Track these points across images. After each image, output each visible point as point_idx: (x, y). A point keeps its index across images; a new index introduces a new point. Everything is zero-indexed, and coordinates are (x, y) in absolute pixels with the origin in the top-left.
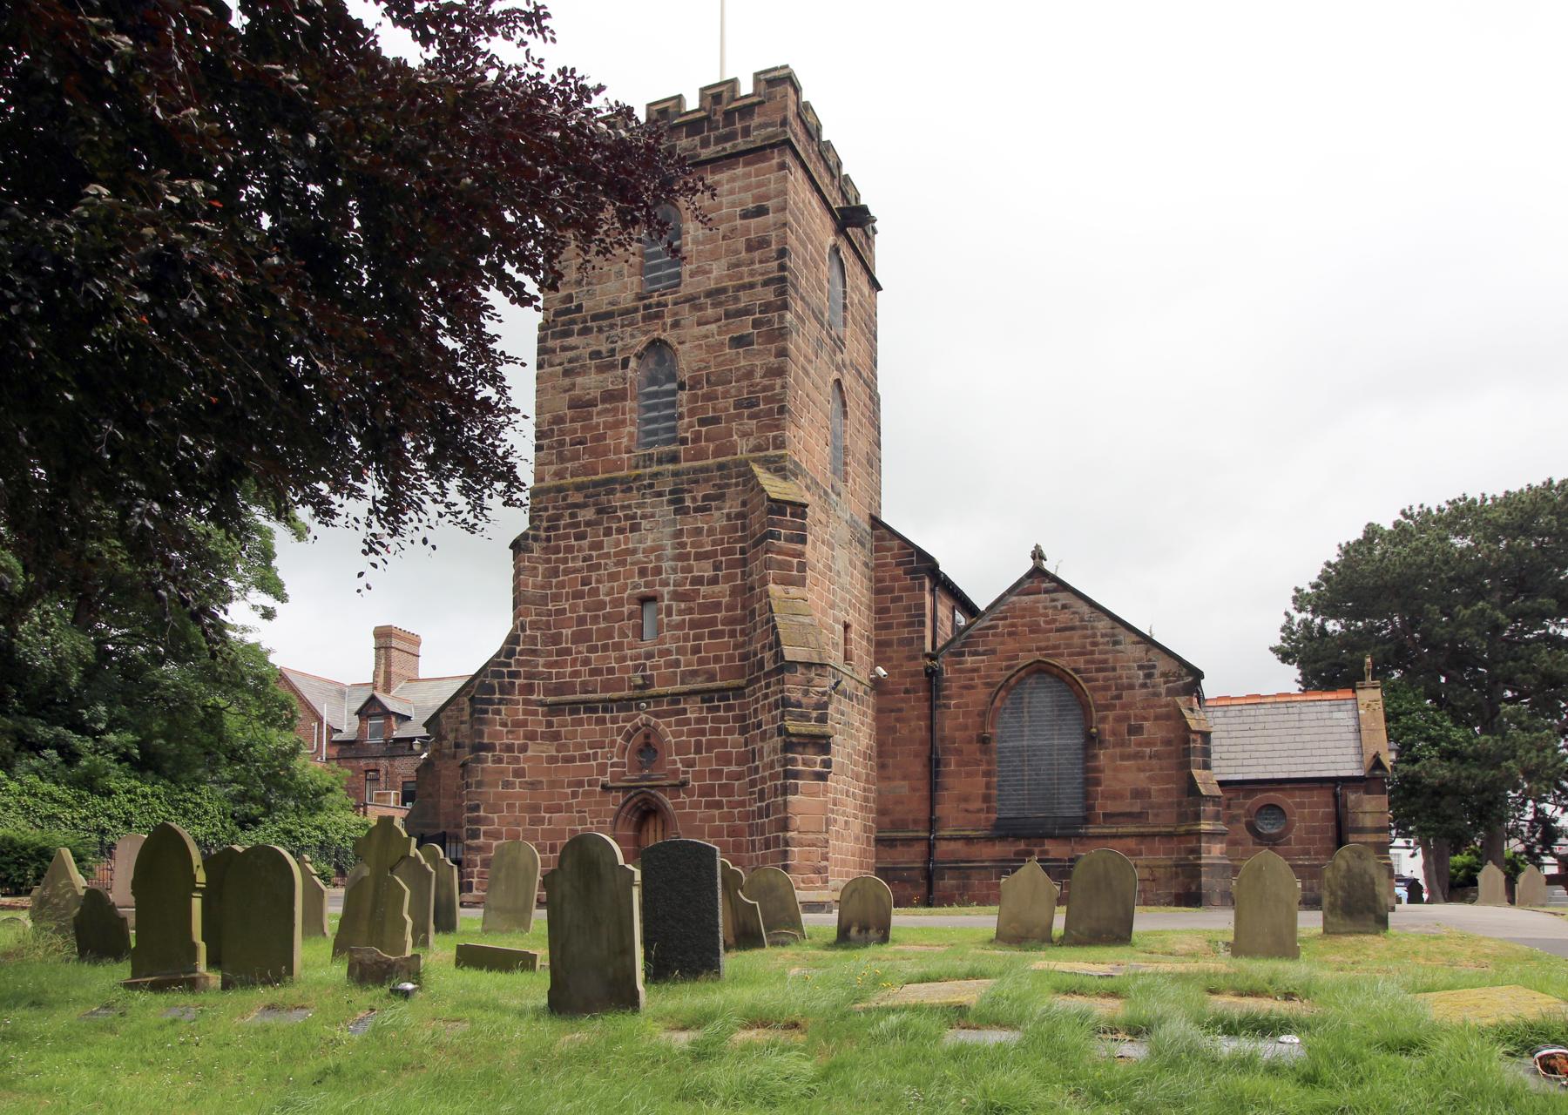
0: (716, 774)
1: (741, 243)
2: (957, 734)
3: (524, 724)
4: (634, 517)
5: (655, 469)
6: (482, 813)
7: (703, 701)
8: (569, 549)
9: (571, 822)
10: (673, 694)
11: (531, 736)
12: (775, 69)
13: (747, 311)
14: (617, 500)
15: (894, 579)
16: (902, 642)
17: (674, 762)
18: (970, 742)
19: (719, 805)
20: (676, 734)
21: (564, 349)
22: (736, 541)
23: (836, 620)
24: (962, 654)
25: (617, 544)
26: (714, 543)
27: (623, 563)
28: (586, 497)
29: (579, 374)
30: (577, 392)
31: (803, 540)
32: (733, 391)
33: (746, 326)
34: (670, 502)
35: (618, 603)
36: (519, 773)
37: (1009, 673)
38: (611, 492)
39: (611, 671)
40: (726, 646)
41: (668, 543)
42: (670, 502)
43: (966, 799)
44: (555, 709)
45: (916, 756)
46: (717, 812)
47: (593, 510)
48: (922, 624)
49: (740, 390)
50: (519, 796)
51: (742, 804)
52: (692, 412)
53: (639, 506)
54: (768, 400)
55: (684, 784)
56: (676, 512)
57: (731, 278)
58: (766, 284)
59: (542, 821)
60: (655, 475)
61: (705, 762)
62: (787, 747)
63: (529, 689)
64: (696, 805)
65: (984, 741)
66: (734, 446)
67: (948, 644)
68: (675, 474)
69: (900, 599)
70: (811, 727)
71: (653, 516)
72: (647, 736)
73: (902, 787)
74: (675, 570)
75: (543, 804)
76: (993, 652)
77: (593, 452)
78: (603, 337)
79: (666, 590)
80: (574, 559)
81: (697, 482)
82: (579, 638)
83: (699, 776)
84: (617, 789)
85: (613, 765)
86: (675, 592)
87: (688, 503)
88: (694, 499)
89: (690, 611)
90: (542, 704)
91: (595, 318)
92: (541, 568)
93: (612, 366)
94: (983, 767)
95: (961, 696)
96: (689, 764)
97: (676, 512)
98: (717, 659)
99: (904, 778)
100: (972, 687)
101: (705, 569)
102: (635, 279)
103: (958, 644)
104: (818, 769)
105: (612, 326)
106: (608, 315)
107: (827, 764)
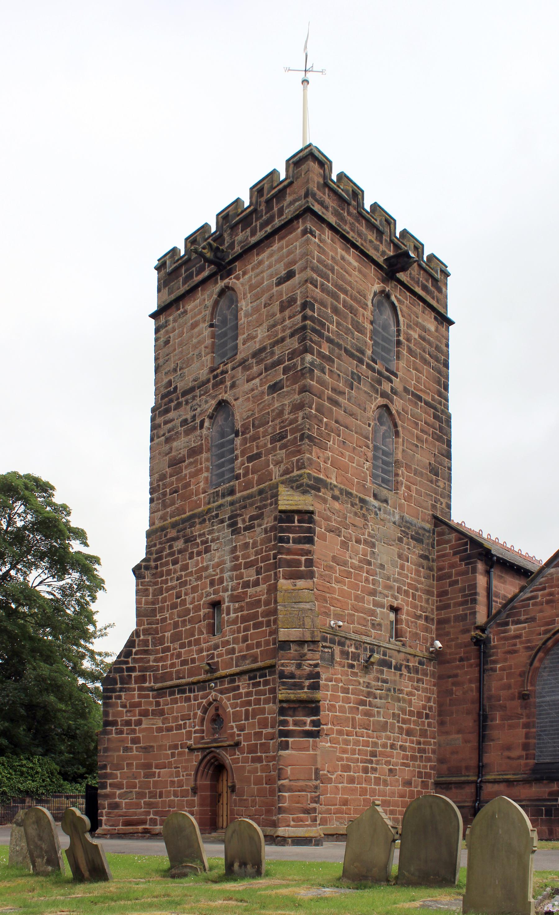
0: (258, 735)
1: (276, 307)
2: (502, 693)
3: (139, 704)
4: (206, 542)
5: (220, 501)
6: (109, 771)
7: (250, 679)
8: (169, 572)
9: (171, 775)
10: (231, 675)
11: (145, 714)
12: (301, 151)
13: (279, 362)
14: (197, 530)
15: (452, 566)
16: (458, 618)
17: (232, 728)
18: (513, 699)
20: (234, 706)
21: (166, 423)
22: (271, 550)
24: (507, 624)
25: (197, 565)
26: (257, 553)
27: (199, 578)
28: (178, 531)
29: (174, 440)
30: (173, 454)
31: (310, 541)
32: (270, 430)
33: (279, 375)
34: (229, 526)
35: (197, 609)
36: (135, 741)
37: (548, 636)
38: (192, 525)
39: (193, 661)
40: (263, 634)
41: (227, 558)
42: (229, 526)
43: (509, 748)
44: (160, 692)
45: (468, 713)
46: (259, 765)
47: (182, 540)
48: (474, 601)
49: (274, 428)
50: (136, 757)
52: (243, 453)
53: (210, 532)
54: (293, 431)
55: (237, 744)
56: (233, 533)
57: (269, 337)
58: (292, 335)
59: (153, 774)
60: (220, 507)
61: (252, 726)
62: (282, 712)
63: (143, 679)
64: (245, 760)
65: (524, 697)
66: (270, 474)
68: (232, 503)
69: (456, 582)
70: (304, 694)
71: (218, 539)
72: (217, 709)
73: (457, 739)
74: (232, 579)
75: (154, 763)
76: (533, 619)
77: (183, 498)
78: (188, 407)
79: (226, 594)
80: (172, 579)
81: (245, 507)
82: (176, 637)
83: (248, 737)
84: (198, 749)
85: (195, 732)
86: (232, 595)
87: (240, 525)
88: (244, 521)
89: (241, 609)
90: (152, 689)
91: (184, 394)
92: (151, 589)
93: (194, 429)
94: (524, 720)
95: (505, 660)
96: (241, 728)
97: (233, 533)
98: (258, 645)
99: (459, 732)
100: (515, 652)
101: (250, 575)
102: (209, 357)
103: (504, 615)
104: (308, 728)
105: (194, 398)
106: (192, 389)
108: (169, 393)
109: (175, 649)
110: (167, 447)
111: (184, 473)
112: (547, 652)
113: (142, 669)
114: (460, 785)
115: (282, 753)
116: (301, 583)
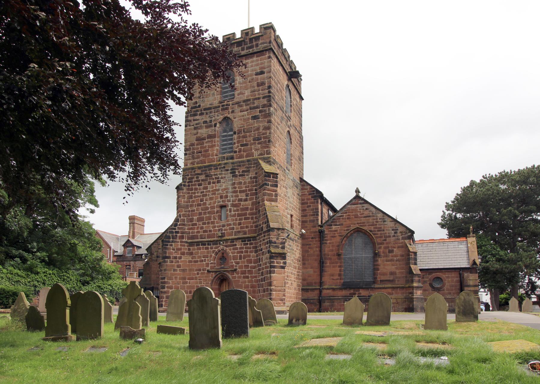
0: (247, 267)
1: (255, 84)
2: (330, 253)
3: (180, 249)
4: (218, 178)
5: (226, 161)
6: (166, 280)
7: (242, 241)
8: (196, 189)
9: (197, 283)
10: (232, 239)
11: (183, 254)
12: (267, 24)
13: (257, 107)
14: (213, 172)
15: (308, 199)
16: (311, 221)
17: (232, 262)
18: (334, 256)
19: (248, 277)
20: (233, 253)
21: (194, 120)
22: (253, 186)
23: (288, 214)
24: (331, 225)
25: (213, 187)
26: (246, 187)
27: (214, 194)
28: (202, 171)
29: (199, 129)
30: (199, 135)
31: (277, 186)
32: (252, 135)
33: (257, 112)
35: (213, 208)
36: (179, 266)
37: (348, 232)
38: (211, 169)
39: (210, 231)
40: (250, 223)
41: (230, 187)
42: (231, 173)
43: (333, 275)
44: (191, 244)
45: (316, 260)
46: (247, 280)
47: (204, 176)
48: (318, 215)
49: (255, 134)
50: (179, 274)
51: (256, 277)
52: (238, 142)
53: (220, 174)
54: (264, 138)
55: (236, 270)
56: (233, 176)
57: (252, 96)
58: (264, 98)
59: (187, 283)
60: (226, 164)
61: (243, 262)
62: (271, 257)
63: (182, 237)
64: (240, 277)
65: (339, 255)
67: (326, 222)
68: (233, 163)
69: (310, 206)
70: (279, 251)
71: (225, 178)
72: (223, 254)
73: (311, 271)
74: (232, 196)
75: (187, 277)
76: (342, 224)
77: (204, 156)
78: (208, 116)
79: (229, 203)
81: (240, 166)
82: (199, 220)
83: (241, 267)
84: (213, 272)
85: (211, 264)
86: (232, 204)
87: (237, 173)
88: (239, 172)
89: (238, 210)
90: (187, 242)
91: (205, 109)
92: (186, 196)
94: (339, 264)
95: (331, 240)
96: (237, 263)
97: (233, 176)
98: (247, 227)
99: (311, 268)
100: (335, 237)
101: (243, 196)
102: (219, 96)
103: (330, 222)
104: (282, 265)
105: (211, 112)
106: (210, 109)
107: (285, 263)
108: (195, 107)
109: (199, 225)
110: (195, 131)
111: (205, 145)
112: (347, 238)
113: (182, 233)
114: (313, 290)
115: (272, 275)
116: (273, 203)
